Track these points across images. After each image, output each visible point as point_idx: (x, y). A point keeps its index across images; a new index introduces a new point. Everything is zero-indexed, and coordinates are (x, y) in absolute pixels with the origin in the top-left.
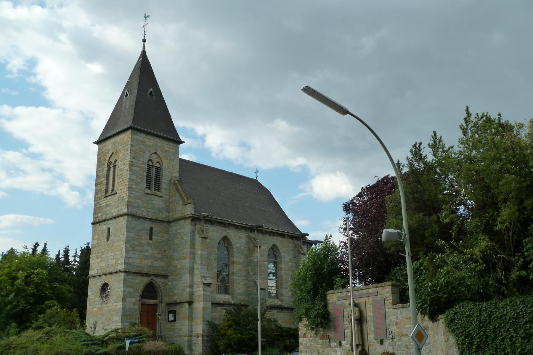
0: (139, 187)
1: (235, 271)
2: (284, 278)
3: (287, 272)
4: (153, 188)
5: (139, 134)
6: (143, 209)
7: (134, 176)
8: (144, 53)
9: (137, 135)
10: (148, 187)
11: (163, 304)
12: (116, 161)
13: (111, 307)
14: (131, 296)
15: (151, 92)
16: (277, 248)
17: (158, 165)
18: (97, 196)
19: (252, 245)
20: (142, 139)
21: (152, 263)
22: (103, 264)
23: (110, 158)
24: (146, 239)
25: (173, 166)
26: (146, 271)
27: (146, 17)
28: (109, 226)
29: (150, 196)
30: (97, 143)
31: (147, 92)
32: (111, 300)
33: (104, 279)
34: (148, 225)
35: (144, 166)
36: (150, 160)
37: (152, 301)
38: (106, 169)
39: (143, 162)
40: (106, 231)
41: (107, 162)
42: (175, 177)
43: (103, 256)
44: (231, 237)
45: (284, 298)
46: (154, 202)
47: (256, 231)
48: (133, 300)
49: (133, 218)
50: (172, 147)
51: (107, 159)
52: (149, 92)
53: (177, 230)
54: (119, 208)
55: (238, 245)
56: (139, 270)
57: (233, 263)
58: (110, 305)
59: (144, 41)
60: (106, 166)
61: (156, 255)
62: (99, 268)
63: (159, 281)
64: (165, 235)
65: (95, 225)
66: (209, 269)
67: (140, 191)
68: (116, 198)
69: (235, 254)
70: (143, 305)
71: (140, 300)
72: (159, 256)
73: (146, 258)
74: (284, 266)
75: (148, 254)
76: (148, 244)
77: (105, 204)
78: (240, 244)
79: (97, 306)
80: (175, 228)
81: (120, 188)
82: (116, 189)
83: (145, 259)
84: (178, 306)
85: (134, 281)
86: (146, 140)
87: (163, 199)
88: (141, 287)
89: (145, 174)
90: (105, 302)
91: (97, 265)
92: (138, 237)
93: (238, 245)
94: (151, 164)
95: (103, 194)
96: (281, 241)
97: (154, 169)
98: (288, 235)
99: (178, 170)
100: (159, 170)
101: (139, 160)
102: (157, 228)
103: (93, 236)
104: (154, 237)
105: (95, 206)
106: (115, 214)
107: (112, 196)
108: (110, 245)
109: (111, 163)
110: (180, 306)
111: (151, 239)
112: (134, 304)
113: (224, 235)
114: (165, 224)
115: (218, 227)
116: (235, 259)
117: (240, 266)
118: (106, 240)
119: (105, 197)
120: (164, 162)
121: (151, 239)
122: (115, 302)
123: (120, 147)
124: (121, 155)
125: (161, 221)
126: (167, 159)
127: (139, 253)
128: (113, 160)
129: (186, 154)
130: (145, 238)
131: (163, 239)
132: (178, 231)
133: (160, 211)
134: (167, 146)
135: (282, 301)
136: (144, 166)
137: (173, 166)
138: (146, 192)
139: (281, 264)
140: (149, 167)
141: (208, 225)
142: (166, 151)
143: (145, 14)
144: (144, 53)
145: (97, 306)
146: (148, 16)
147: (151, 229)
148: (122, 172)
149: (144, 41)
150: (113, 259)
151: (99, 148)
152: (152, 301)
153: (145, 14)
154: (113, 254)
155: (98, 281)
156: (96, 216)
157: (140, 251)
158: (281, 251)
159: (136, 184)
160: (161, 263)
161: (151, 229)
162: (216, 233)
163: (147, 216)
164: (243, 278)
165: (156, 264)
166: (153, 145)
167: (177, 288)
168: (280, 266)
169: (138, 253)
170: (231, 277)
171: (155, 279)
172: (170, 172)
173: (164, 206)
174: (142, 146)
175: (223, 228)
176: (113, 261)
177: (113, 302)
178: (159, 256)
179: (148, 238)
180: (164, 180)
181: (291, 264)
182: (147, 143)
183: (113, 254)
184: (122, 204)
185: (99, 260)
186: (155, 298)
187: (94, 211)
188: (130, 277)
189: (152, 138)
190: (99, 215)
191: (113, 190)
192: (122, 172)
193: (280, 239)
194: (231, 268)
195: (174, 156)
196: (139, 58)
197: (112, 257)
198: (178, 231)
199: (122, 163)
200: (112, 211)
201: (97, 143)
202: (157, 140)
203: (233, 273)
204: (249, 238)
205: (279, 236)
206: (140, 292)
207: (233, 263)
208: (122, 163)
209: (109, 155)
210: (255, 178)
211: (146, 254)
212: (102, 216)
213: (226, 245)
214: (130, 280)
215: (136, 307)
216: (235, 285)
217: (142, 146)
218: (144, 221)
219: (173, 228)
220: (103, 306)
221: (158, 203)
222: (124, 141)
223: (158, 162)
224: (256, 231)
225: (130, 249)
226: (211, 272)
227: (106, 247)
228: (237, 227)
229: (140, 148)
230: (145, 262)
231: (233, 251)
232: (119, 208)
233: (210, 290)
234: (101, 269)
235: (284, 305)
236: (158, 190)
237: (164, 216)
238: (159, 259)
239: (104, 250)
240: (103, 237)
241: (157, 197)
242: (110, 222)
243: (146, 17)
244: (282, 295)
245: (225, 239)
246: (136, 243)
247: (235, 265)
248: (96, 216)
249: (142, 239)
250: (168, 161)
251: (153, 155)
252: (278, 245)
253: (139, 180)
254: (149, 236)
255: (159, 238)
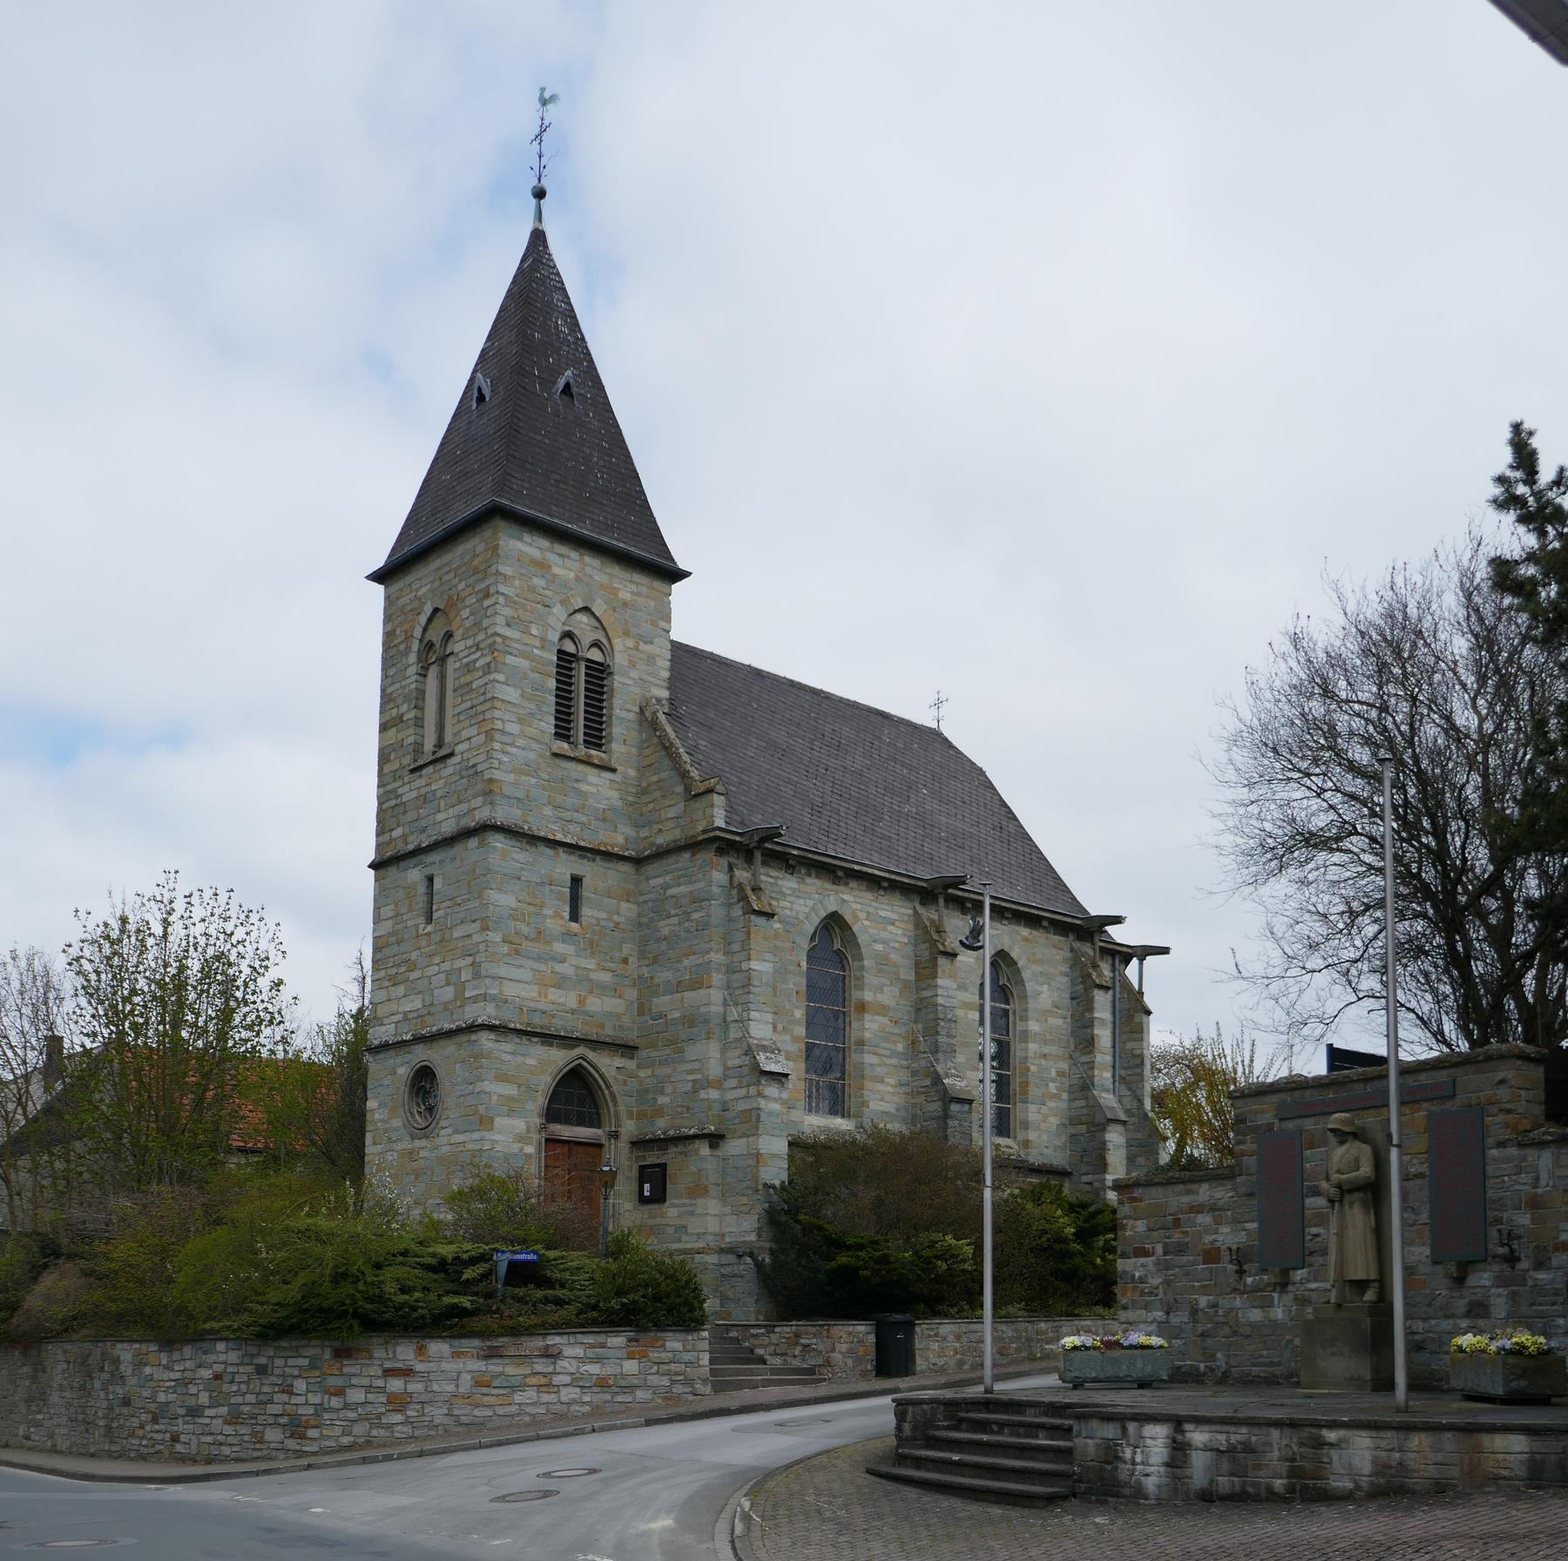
0: (530, 731)
1: (867, 1035)
2: (1033, 1068)
3: (1046, 1050)
4: (581, 737)
5: (527, 537)
6: (548, 811)
7: (510, 690)
8: (538, 238)
9: (521, 540)
10: (563, 732)
11: (623, 1145)
12: (448, 636)
13: (445, 1149)
14: (510, 1113)
15: (567, 385)
16: (1012, 963)
17: (595, 655)
18: (386, 770)
19: (931, 954)
20: (536, 554)
21: (581, 1002)
22: (414, 1004)
23: (425, 629)
24: (557, 915)
25: (651, 659)
26: (560, 1025)
27: (544, 102)
28: (428, 871)
29: (571, 765)
30: (379, 577)
31: (554, 383)
32: (442, 1123)
33: (420, 1054)
34: (564, 867)
35: (545, 655)
36: (568, 635)
37: (566, 1131)
38: (412, 670)
39: (543, 639)
40: (422, 889)
41: (415, 646)
42: (659, 701)
43: (413, 975)
44: (856, 918)
45: (1032, 1136)
46: (584, 787)
47: (941, 901)
48: (519, 1125)
49: (513, 842)
50: (644, 590)
51: (418, 633)
52: (561, 382)
53: (666, 887)
54: (464, 807)
55: (879, 947)
56: (539, 1022)
57: (862, 1008)
58: (442, 1140)
59: (540, 194)
60: (413, 658)
61: (592, 976)
62: (400, 1017)
63: (607, 1065)
64: (624, 905)
65: (383, 872)
66: (780, 1027)
67: (535, 746)
68: (450, 770)
69: (871, 978)
70: (551, 1142)
71: (543, 1128)
72: (606, 977)
73: (560, 982)
74: (1034, 1026)
75: (565, 969)
76: (568, 936)
77: (414, 794)
78: (885, 942)
79: (399, 1146)
80: (660, 881)
81: (465, 734)
82: (448, 738)
83: (558, 986)
84: (672, 1150)
85: (520, 1058)
86: (552, 558)
87: (617, 777)
88: (545, 1081)
89: (552, 684)
90: (425, 1132)
91: (393, 1007)
92: (532, 909)
93: (879, 947)
94: (569, 647)
95: (407, 760)
96: (1026, 940)
97: (583, 670)
98: (1052, 922)
99: (666, 674)
100: (599, 674)
101: (527, 632)
102: (596, 876)
103: (377, 909)
104: (586, 911)
105: (380, 804)
106: (448, 828)
107: (439, 766)
108: (436, 938)
109: (430, 645)
110: (681, 1148)
111: (575, 916)
112: (520, 1139)
113: (832, 909)
114: (625, 867)
115: (808, 880)
116: (868, 996)
117: (885, 1020)
118: (422, 920)
119: (412, 771)
120: (618, 643)
121: (575, 916)
122: (457, 1132)
123: (461, 586)
124: (465, 613)
125: (608, 856)
126: (627, 634)
127: (536, 965)
128: (435, 635)
129: (700, 617)
130: (554, 915)
131: (616, 918)
132: (670, 892)
133: (604, 820)
134: (629, 586)
135: (1026, 1144)
136: (545, 655)
137: (651, 659)
138: (555, 750)
139: (1025, 1019)
140: (565, 660)
141: (774, 873)
142: (625, 604)
143: (543, 90)
144: (538, 238)
145: (399, 1146)
146: (553, 98)
147: (576, 881)
148: (468, 678)
149: (540, 194)
150: (448, 984)
151: (387, 598)
152: (566, 1131)
153: (543, 90)
154: (446, 966)
155: (399, 1060)
156: (386, 837)
157: (539, 959)
158: (1026, 975)
159: (520, 720)
160: (612, 1004)
161: (576, 881)
162: (801, 901)
163: (559, 837)
164: (894, 1061)
165: (595, 1004)
166: (577, 579)
167: (668, 1090)
168: (1020, 1026)
169: (530, 962)
170: (854, 1058)
171: (591, 1055)
172: (637, 683)
173: (620, 803)
174: (538, 582)
175: (829, 886)
176: (448, 993)
177: (449, 1131)
178: (606, 977)
179: (566, 915)
180: (617, 711)
181: (1059, 1022)
182: (556, 570)
183: (446, 966)
184: (470, 792)
185: (400, 990)
186: (595, 1122)
187: (379, 822)
188: (508, 1047)
189: (574, 555)
190: (397, 833)
191: (440, 744)
192: (468, 678)
193: (1025, 932)
194: (855, 1025)
195: (653, 623)
196: (523, 260)
197: (443, 976)
198: (670, 892)
199: (470, 642)
200: (440, 817)
201: (379, 577)
202: (591, 562)
203: (861, 1043)
204: (918, 921)
205: (1018, 923)
206: (539, 1101)
207: (862, 1008)
208: (470, 642)
209: (423, 619)
210: (934, 725)
211: (559, 968)
212: (404, 837)
213: (837, 945)
214: (508, 1057)
215: (530, 1149)
216: (868, 1084)
217: (538, 582)
218: (549, 851)
219: (653, 882)
220: (418, 1143)
221: (599, 789)
222: (476, 562)
223: (596, 644)
224: (941, 901)
225: (505, 949)
226: (787, 1038)
227: (424, 943)
228: (874, 883)
229: (532, 589)
230: (554, 995)
231: (862, 968)
232: (464, 807)
233: (785, 1095)
234: (405, 1019)
235: (1031, 1160)
236: (599, 746)
237: (620, 839)
238: (603, 989)
239: (414, 955)
240: (410, 910)
241: (595, 771)
242: (434, 857)
243: (544, 102)
244: (1025, 1125)
245: (834, 924)
246: (525, 930)
247: (867, 1016)
248: (386, 837)
249: (545, 917)
250: (630, 643)
251: (579, 616)
252: (1014, 955)
253: (532, 706)
254: (567, 908)
255: (604, 916)
